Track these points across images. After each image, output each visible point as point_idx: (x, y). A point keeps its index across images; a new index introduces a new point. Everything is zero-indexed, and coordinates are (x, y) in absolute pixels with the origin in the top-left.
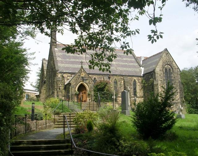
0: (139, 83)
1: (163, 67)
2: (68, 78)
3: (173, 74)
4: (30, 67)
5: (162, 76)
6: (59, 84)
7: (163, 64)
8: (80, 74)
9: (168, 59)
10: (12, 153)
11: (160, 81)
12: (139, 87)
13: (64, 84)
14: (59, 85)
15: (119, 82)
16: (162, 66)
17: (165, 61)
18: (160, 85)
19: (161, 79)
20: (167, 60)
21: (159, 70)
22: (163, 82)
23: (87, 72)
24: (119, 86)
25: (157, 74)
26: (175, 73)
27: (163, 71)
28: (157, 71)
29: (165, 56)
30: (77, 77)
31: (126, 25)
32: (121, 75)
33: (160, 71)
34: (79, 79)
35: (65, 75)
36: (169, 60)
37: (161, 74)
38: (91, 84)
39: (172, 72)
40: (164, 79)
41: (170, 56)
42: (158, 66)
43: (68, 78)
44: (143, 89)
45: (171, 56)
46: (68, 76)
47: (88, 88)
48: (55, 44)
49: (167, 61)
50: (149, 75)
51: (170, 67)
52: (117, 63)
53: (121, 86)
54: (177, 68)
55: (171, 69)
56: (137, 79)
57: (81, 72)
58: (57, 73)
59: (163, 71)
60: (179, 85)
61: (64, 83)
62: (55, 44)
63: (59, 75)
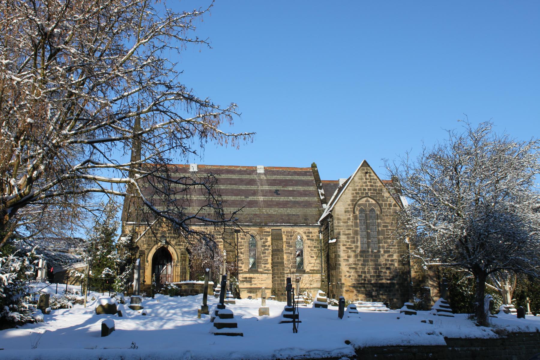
0: (309, 242)
1: (355, 203)
3: (381, 219)
4: (206, 146)
5: (350, 223)
7: (353, 197)
9: (369, 184)
11: (346, 235)
12: (309, 249)
15: (261, 239)
16: (353, 201)
17: (360, 189)
18: (344, 245)
19: (347, 232)
20: (367, 186)
21: (343, 210)
22: (353, 238)
24: (260, 248)
25: (339, 219)
26: (387, 215)
27: (354, 213)
28: (336, 213)
29: (362, 179)
31: (147, 185)
33: (346, 212)
36: (371, 186)
37: (349, 219)
38: (181, 247)
41: (375, 177)
45: (378, 177)
47: (175, 256)
51: (374, 202)
52: (266, 198)
53: (265, 249)
56: (305, 233)
59: (354, 213)
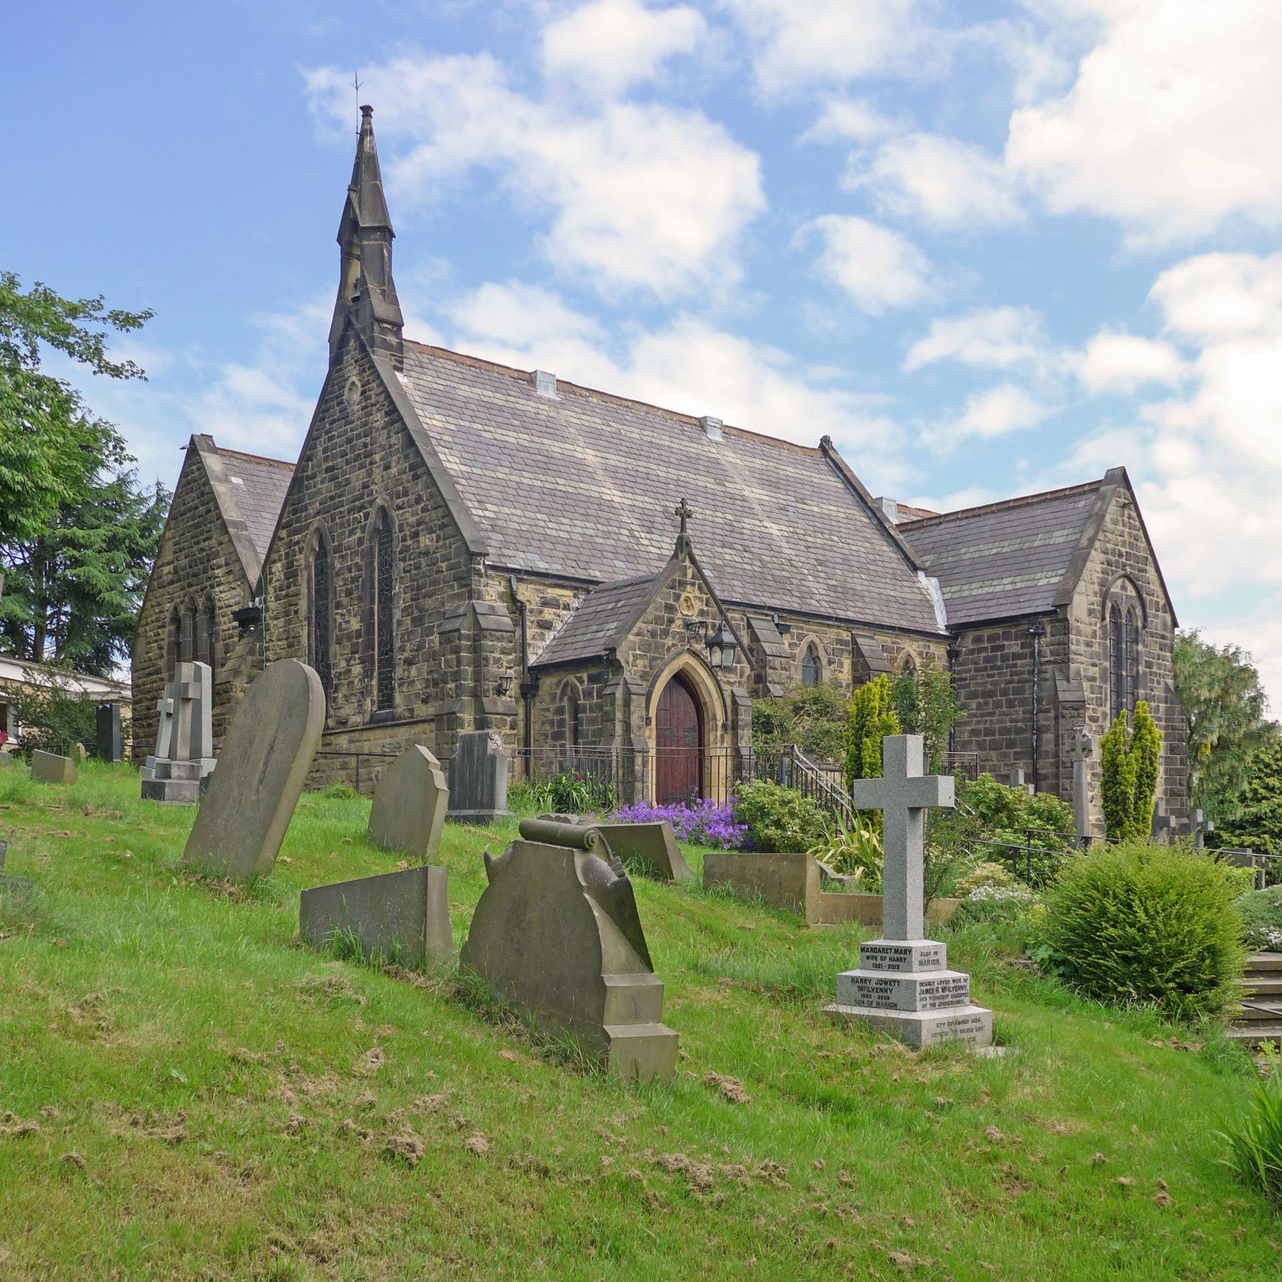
2: (548, 614)
5: (1096, 648)
6: (497, 661)
8: (677, 597)
10: (1268, 1170)
13: (523, 659)
14: (493, 669)
23: (717, 593)
25: (1079, 633)
30: (658, 620)
32: (838, 619)
34: (666, 633)
35: (526, 593)
37: (1094, 634)
39: (1140, 625)
40: (1105, 669)
42: (1081, 586)
43: (548, 614)
44: (104, 671)
46: (546, 603)
48: (392, 339)
49: (1120, 555)
50: (1007, 636)
51: (1134, 594)
54: (1162, 602)
55: (1139, 612)
56: (920, 654)
57: (682, 584)
58: (479, 574)
60: (1167, 711)
61: (524, 651)
62: (392, 339)
63: (492, 592)
